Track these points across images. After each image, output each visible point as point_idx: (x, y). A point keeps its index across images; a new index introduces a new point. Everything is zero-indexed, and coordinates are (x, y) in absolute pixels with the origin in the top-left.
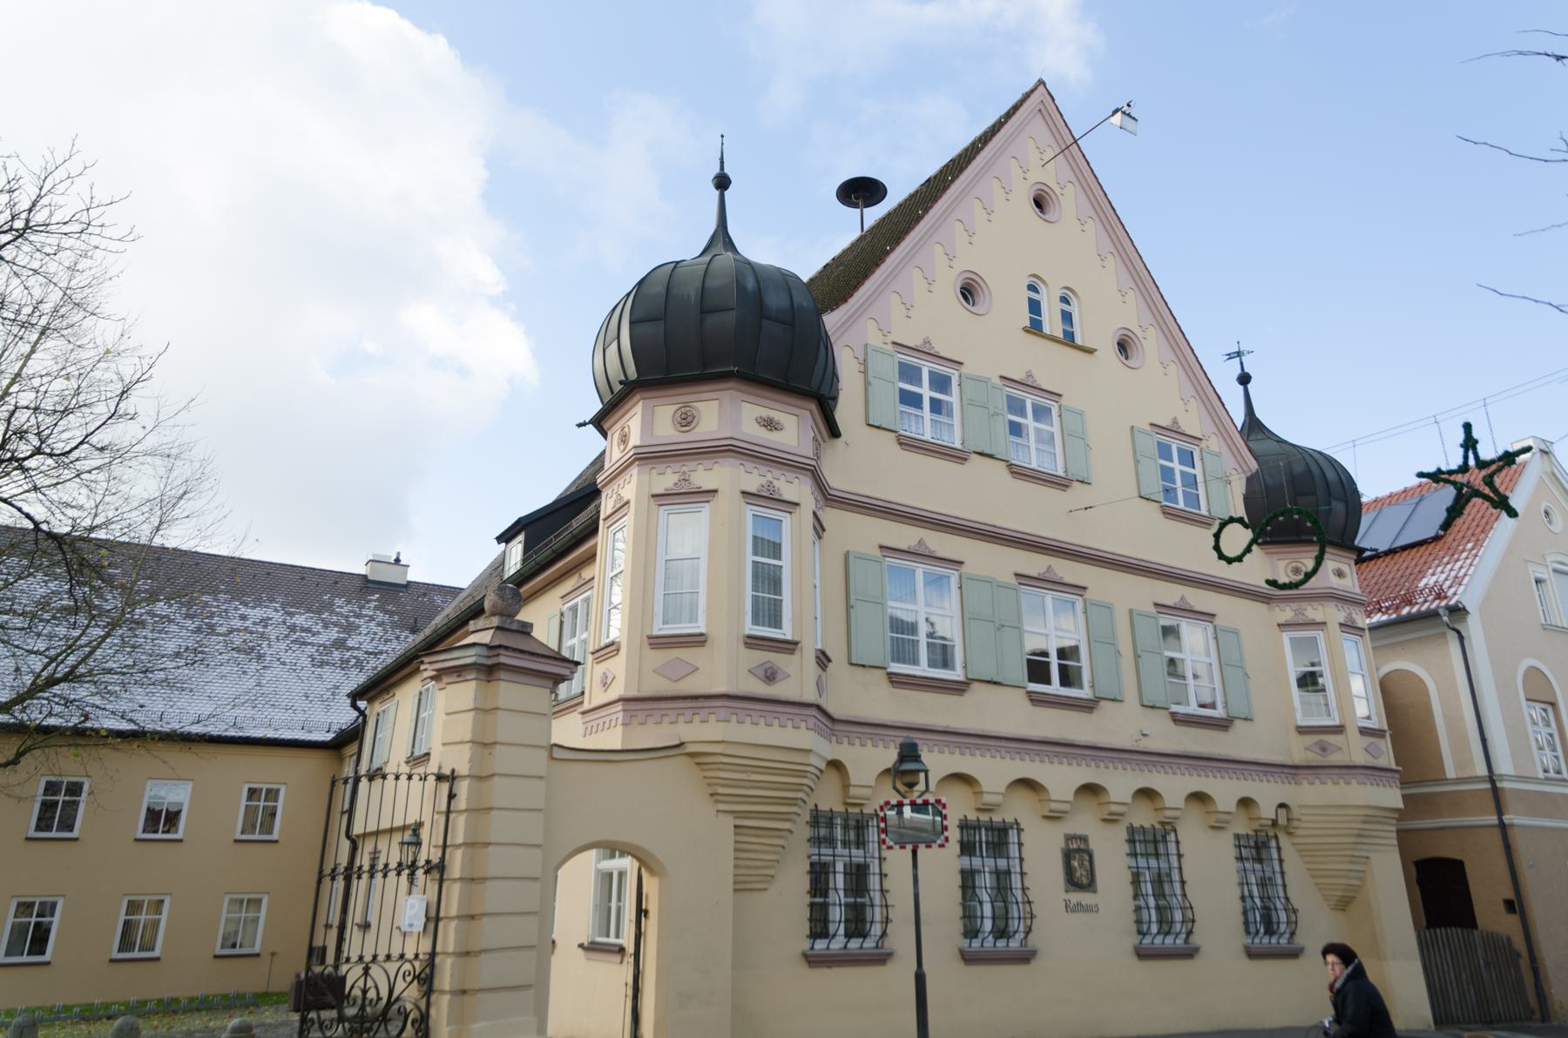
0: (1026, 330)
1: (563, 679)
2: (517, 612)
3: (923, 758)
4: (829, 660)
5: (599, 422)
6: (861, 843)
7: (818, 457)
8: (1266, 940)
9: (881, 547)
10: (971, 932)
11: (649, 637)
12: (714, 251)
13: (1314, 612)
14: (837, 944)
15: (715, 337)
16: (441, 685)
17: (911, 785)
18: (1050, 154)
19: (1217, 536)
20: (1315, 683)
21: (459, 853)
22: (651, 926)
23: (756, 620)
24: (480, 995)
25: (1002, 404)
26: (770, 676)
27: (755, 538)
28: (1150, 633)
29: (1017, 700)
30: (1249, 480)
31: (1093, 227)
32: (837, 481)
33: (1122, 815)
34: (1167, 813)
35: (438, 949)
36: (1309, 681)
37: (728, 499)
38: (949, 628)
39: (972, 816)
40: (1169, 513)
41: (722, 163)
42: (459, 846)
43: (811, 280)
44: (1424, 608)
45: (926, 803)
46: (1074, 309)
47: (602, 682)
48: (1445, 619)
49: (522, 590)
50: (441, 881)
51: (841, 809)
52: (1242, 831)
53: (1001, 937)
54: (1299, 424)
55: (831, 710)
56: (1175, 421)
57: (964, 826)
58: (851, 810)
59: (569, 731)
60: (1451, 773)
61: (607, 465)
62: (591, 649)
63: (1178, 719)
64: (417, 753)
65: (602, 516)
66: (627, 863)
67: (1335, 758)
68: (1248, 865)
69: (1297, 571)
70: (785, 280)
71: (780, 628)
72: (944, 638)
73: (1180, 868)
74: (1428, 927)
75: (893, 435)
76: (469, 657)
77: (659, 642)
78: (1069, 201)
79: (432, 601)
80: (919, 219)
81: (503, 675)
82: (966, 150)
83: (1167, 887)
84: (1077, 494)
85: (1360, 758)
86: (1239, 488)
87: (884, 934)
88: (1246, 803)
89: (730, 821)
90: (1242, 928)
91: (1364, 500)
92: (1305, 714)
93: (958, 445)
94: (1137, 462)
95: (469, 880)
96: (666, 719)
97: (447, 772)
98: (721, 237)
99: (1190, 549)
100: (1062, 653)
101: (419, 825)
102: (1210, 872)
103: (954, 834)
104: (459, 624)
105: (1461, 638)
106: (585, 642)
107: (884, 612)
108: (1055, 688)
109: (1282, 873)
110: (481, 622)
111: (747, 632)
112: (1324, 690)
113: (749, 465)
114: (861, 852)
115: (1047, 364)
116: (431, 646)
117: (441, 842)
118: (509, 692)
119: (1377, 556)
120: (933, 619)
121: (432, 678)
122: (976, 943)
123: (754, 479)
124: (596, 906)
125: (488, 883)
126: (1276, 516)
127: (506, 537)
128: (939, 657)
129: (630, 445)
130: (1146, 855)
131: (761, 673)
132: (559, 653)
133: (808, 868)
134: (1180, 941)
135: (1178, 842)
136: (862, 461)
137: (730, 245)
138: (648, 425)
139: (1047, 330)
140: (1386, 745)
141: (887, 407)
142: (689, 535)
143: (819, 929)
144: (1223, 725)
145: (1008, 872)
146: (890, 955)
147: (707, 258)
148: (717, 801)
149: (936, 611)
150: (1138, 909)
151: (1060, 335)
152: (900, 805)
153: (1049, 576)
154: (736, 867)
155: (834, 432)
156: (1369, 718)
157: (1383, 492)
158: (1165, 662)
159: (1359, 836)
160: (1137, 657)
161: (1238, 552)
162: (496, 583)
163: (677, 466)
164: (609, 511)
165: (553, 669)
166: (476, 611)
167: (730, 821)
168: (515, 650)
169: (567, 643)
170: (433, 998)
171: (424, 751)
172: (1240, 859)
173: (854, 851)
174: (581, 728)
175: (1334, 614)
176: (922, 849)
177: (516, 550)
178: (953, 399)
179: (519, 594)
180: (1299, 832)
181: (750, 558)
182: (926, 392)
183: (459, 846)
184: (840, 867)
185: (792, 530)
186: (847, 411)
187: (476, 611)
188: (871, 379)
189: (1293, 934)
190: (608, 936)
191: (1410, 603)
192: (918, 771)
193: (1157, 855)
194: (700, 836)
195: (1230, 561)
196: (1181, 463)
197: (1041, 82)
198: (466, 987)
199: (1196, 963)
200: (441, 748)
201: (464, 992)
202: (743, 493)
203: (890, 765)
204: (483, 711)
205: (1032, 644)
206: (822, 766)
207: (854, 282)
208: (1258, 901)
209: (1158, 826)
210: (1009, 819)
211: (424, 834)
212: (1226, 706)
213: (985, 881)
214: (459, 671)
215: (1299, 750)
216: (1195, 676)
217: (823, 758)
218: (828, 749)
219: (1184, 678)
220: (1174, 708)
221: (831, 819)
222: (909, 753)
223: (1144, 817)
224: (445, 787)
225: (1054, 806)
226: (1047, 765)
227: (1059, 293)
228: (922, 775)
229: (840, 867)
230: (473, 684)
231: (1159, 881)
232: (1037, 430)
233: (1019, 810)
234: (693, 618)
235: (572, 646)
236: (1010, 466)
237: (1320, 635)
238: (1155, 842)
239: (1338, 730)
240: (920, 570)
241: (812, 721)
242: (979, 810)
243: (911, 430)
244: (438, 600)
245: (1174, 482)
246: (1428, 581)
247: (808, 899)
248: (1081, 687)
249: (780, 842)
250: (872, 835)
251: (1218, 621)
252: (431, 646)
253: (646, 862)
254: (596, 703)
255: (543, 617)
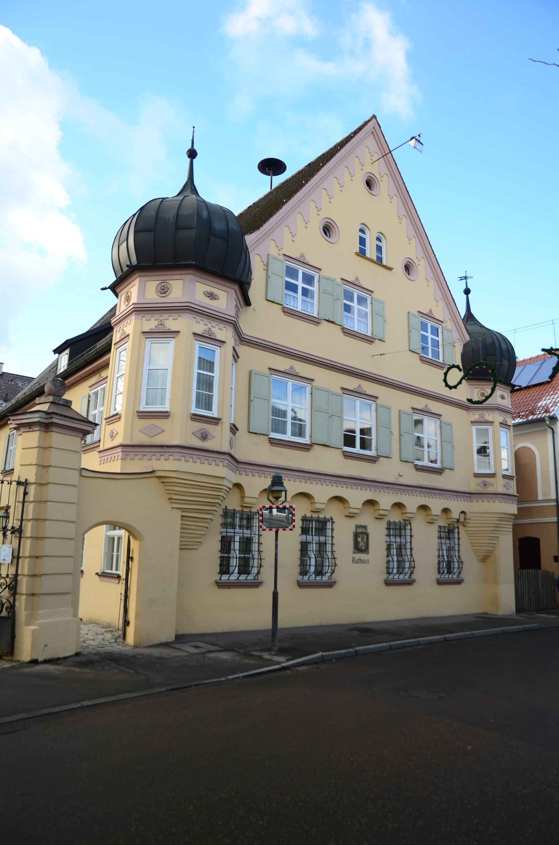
0: (357, 254)
1: (88, 433)
2: (63, 394)
3: (284, 484)
4: (237, 430)
5: (114, 288)
6: (249, 527)
7: (237, 316)
8: (447, 576)
9: (270, 369)
10: (304, 572)
11: (137, 412)
12: (185, 194)
13: (489, 416)
14: (234, 577)
15: (182, 243)
16: (20, 433)
17: (277, 498)
18: (376, 157)
19: (446, 374)
20: (485, 452)
21: (30, 524)
22: (135, 566)
23: (198, 406)
24: (42, 597)
25: (341, 294)
26: (204, 437)
27: (200, 358)
28: (408, 423)
29: (338, 454)
30: (465, 346)
31: (396, 200)
32: (247, 330)
33: (385, 516)
34: (408, 515)
35: (19, 573)
36: (482, 451)
37: (185, 337)
38: (304, 414)
39: (309, 515)
40: (424, 360)
41: (193, 143)
42: (30, 520)
43: (241, 215)
44: (539, 417)
45: (285, 508)
46: (383, 245)
47: (108, 435)
48: (548, 422)
49: (66, 382)
50: (20, 538)
51: (240, 509)
52: (442, 525)
53: (319, 575)
54: (490, 319)
55: (237, 456)
56: (431, 311)
57: (304, 519)
58: (245, 510)
59: (91, 461)
60: (540, 497)
61: (117, 313)
62: (105, 417)
63: (418, 468)
64: (7, 469)
65: (113, 342)
66: (122, 533)
67: (490, 490)
68: (443, 541)
69: (483, 394)
70: (225, 213)
71: (211, 410)
72: (301, 420)
73: (411, 542)
74: (520, 569)
75: (280, 306)
76: (35, 418)
77: (143, 415)
78: (384, 184)
79: (16, 384)
80: (302, 186)
81: (54, 429)
82: (331, 149)
83: (403, 551)
84: (378, 347)
85: (501, 490)
86: (459, 349)
87: (259, 573)
88: (446, 511)
89: (179, 513)
90: (436, 570)
91: (517, 360)
92: (478, 468)
93: (315, 315)
94: (410, 331)
95: (36, 538)
96: (145, 457)
97: (23, 480)
98: (190, 186)
99: (431, 380)
100: (362, 431)
101: (8, 507)
102: (425, 543)
103: (298, 524)
104: (30, 399)
105: (553, 432)
106: (102, 412)
107: (412, 417)
108: (357, 450)
109: (459, 544)
110: (42, 399)
111: (193, 412)
112: (489, 456)
113: (199, 318)
114: (249, 531)
115: (367, 274)
116: (15, 410)
117: (20, 518)
118: (58, 438)
119: (521, 389)
120: (296, 410)
121: (15, 428)
122: (306, 578)
123: (200, 326)
124: (105, 554)
125: (46, 540)
126: (475, 366)
127: (59, 350)
128: (297, 430)
129: (131, 303)
130: (395, 536)
131: (199, 435)
132: (87, 419)
133: (220, 538)
134: (406, 577)
135: (411, 530)
136: (262, 320)
137: (194, 191)
138: (142, 291)
139: (368, 255)
140: (513, 483)
141: (278, 290)
142: (163, 355)
143: (224, 568)
144: (439, 472)
145: (325, 543)
146: (261, 583)
147: (181, 198)
148: (172, 503)
149: (296, 403)
150: (388, 562)
151: (375, 258)
152: (271, 508)
153: (358, 390)
154: (181, 537)
155: (247, 303)
156: (507, 470)
157: (527, 357)
158: (415, 438)
159: (496, 527)
160: (400, 435)
161: (455, 384)
162: (52, 376)
163: (157, 316)
164: (118, 340)
165: (83, 427)
166: (40, 392)
167: (179, 513)
168: (61, 415)
169: (92, 412)
170: (17, 597)
171: (11, 468)
172: (440, 538)
173: (245, 531)
174: (98, 460)
175: (498, 417)
176: (281, 531)
177: (64, 358)
178: (315, 289)
179: (64, 384)
180: (469, 525)
181: (196, 371)
182: (300, 284)
183: (30, 520)
184: (237, 539)
185: (220, 357)
186: (256, 291)
187: (40, 392)
188: (270, 274)
189: (460, 573)
190: (112, 569)
191: (533, 414)
192: (282, 491)
193: (400, 536)
194: (163, 521)
195: (451, 388)
196: (427, 337)
197: (374, 117)
198: (35, 592)
199: (413, 587)
200: (20, 467)
201: (33, 595)
202: (194, 334)
203: (267, 487)
204: (43, 448)
205: (347, 425)
206: (231, 486)
207: (264, 218)
208: (445, 558)
209: (402, 522)
210: (328, 517)
211: (11, 511)
212: (442, 463)
213: (313, 547)
214: (30, 425)
215: (474, 486)
216: (429, 446)
217: (231, 482)
218: (233, 477)
219: (423, 447)
220: (417, 462)
221: (234, 514)
222: (277, 481)
223: (396, 517)
224: (22, 488)
225: (351, 510)
226: (349, 490)
227: (376, 235)
228: (283, 493)
229: (237, 539)
230: (38, 433)
231: (400, 548)
232: (359, 310)
233: (334, 512)
234: (163, 403)
235: (95, 415)
236: (343, 328)
237: (490, 428)
238: (400, 529)
239: (493, 475)
240: (290, 383)
241: (226, 462)
242: (313, 511)
243: (290, 304)
244: (20, 384)
245: (427, 344)
246: (542, 403)
247: (219, 555)
248: (371, 450)
249: (206, 525)
250: (256, 523)
251: (442, 418)
252: (15, 410)
253: (132, 533)
254: (106, 447)
255: (78, 398)
